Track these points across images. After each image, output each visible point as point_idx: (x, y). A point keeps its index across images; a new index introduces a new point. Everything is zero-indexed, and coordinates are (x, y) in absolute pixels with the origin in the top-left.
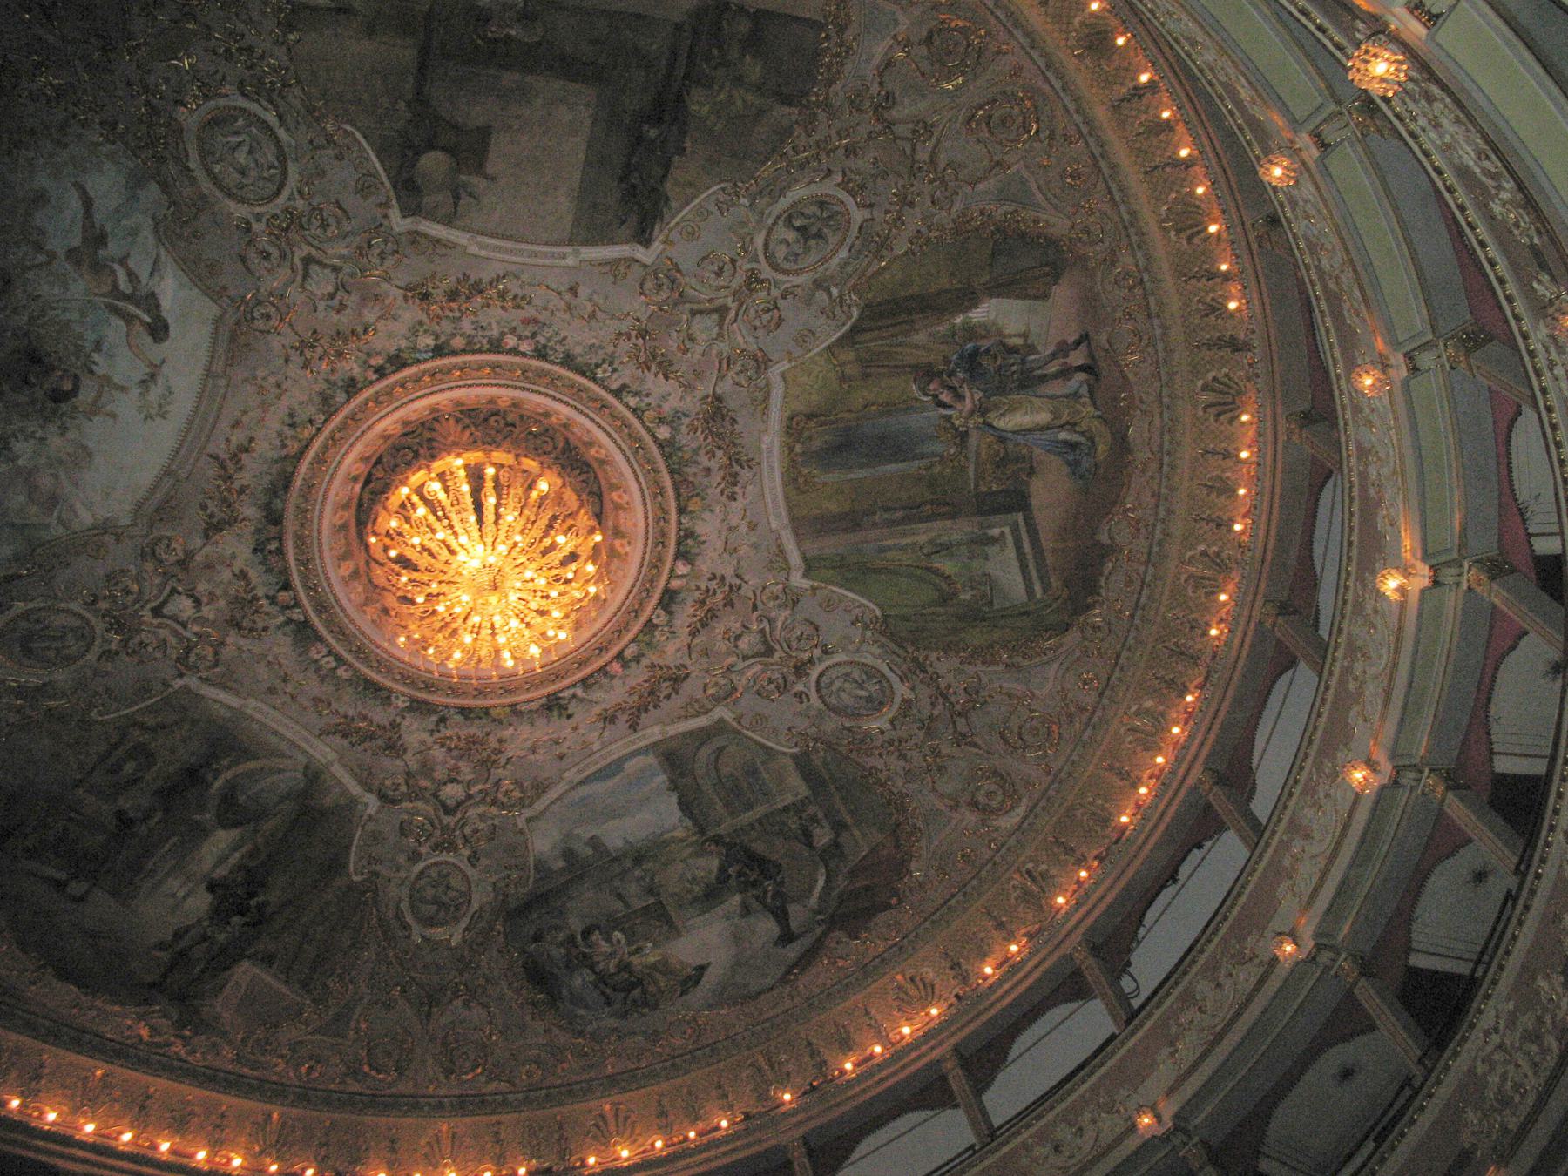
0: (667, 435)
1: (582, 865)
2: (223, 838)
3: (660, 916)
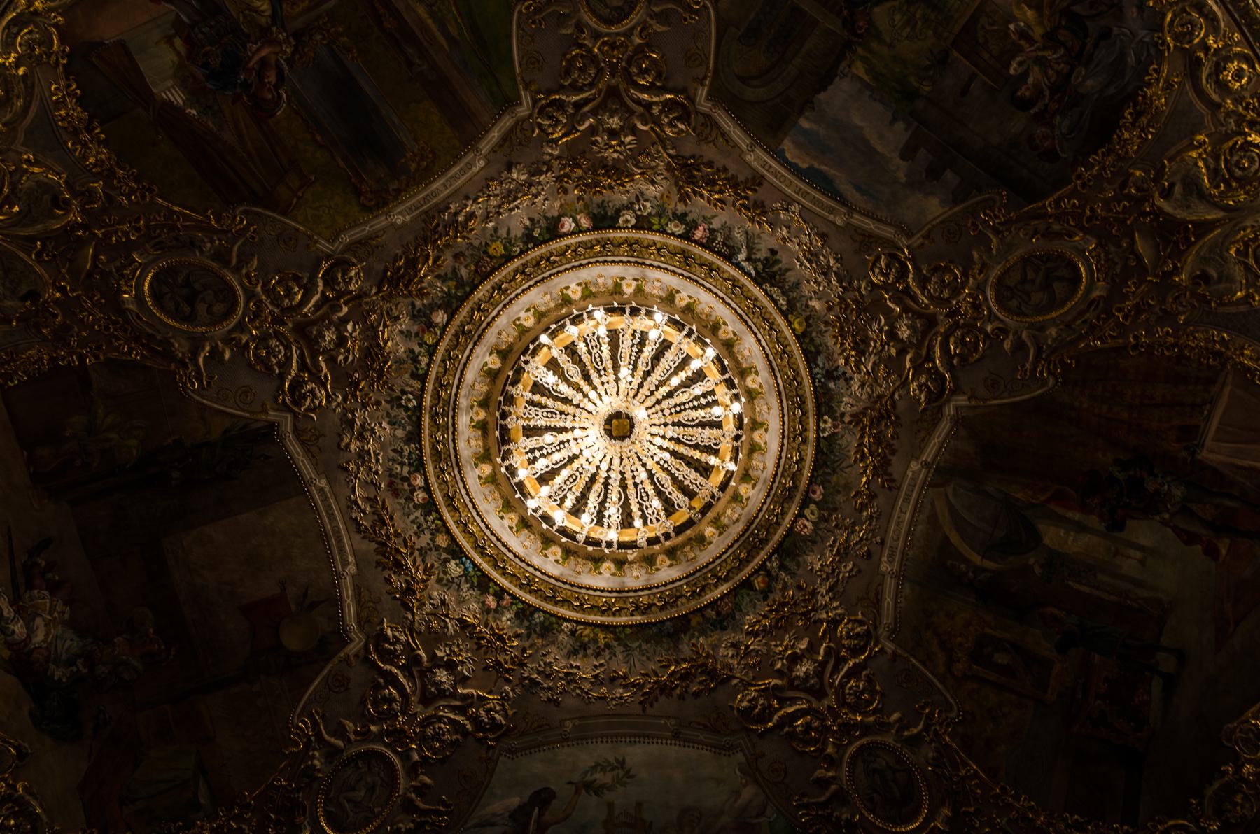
0: (441, 313)
2: (1052, 536)
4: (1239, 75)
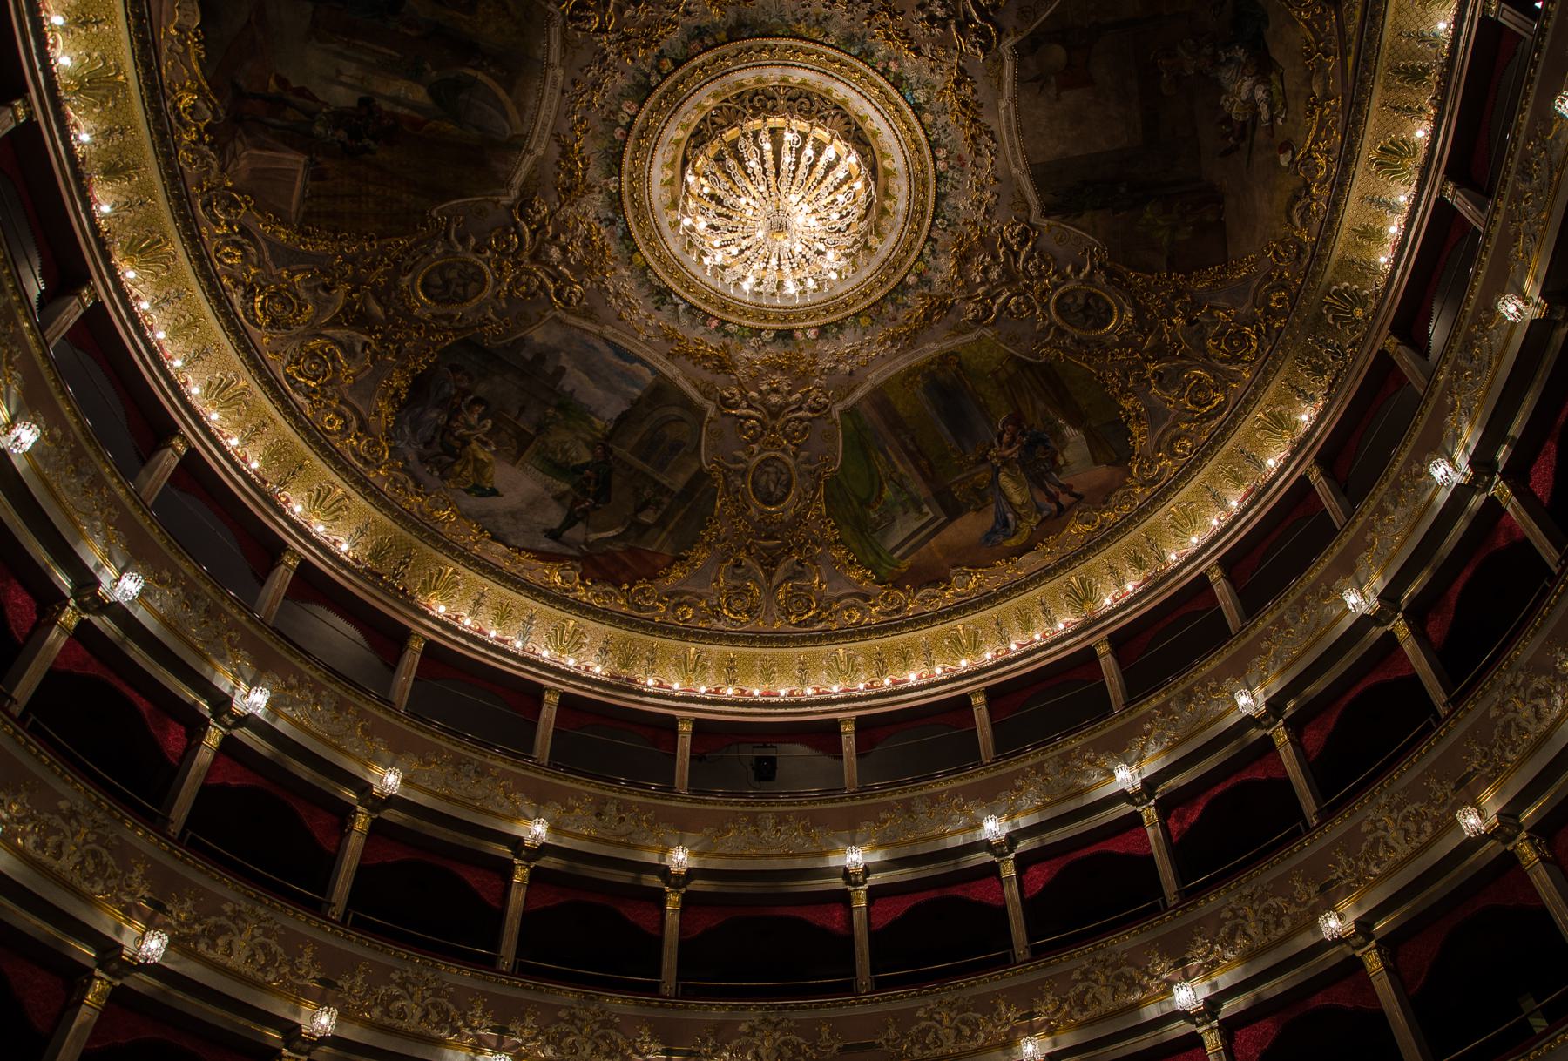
1: (537, 376)
2: (420, 95)
3: (519, 445)
4: (331, 423)
